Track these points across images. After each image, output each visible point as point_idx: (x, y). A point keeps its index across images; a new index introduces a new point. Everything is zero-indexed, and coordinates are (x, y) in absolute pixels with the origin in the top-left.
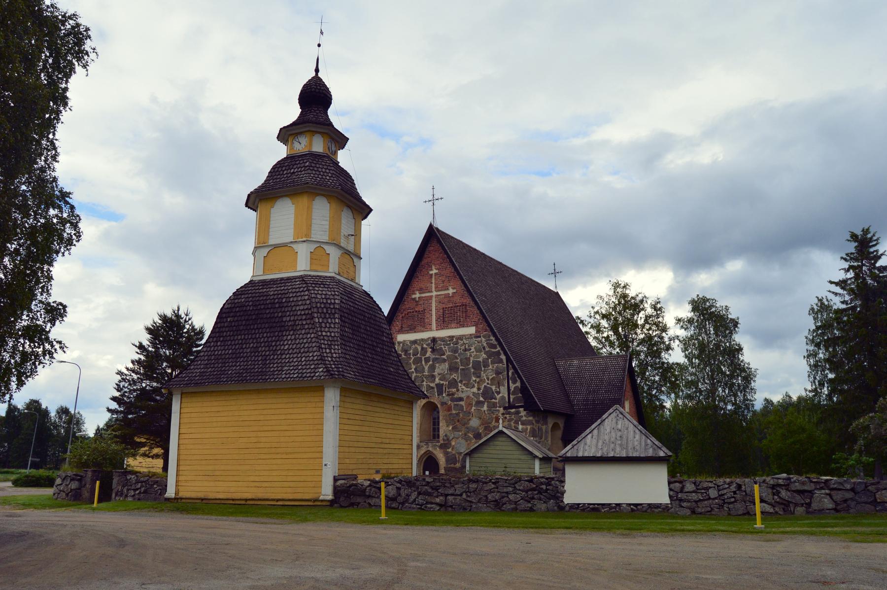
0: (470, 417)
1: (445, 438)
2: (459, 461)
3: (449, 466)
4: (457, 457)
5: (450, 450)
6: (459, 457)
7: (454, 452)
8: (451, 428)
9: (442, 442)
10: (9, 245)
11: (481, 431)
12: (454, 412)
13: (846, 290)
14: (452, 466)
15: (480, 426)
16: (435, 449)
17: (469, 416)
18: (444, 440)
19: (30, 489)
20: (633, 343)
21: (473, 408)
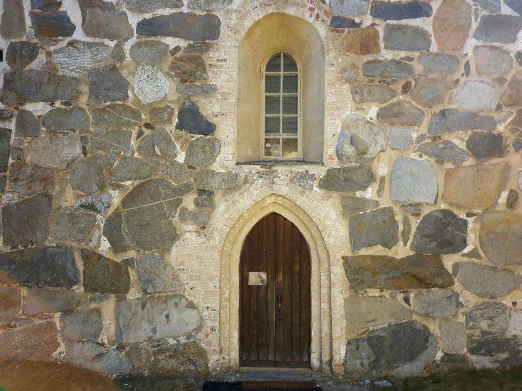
0: (457, 75)
1: (349, 150)
2: (405, 235)
3: (364, 252)
4: (399, 218)
5: (370, 193)
6: (406, 221)
7: (385, 203)
8: (373, 111)
9: (335, 164)
10: (146, 375)
11: (501, 128)
12: (387, 55)
13: (171, 222)
14: (378, 250)
15: (499, 108)
16: (305, 190)
17: (451, 71)
18: (339, 155)
19: (313, 270)
20: (75, 241)
21: (471, 43)
